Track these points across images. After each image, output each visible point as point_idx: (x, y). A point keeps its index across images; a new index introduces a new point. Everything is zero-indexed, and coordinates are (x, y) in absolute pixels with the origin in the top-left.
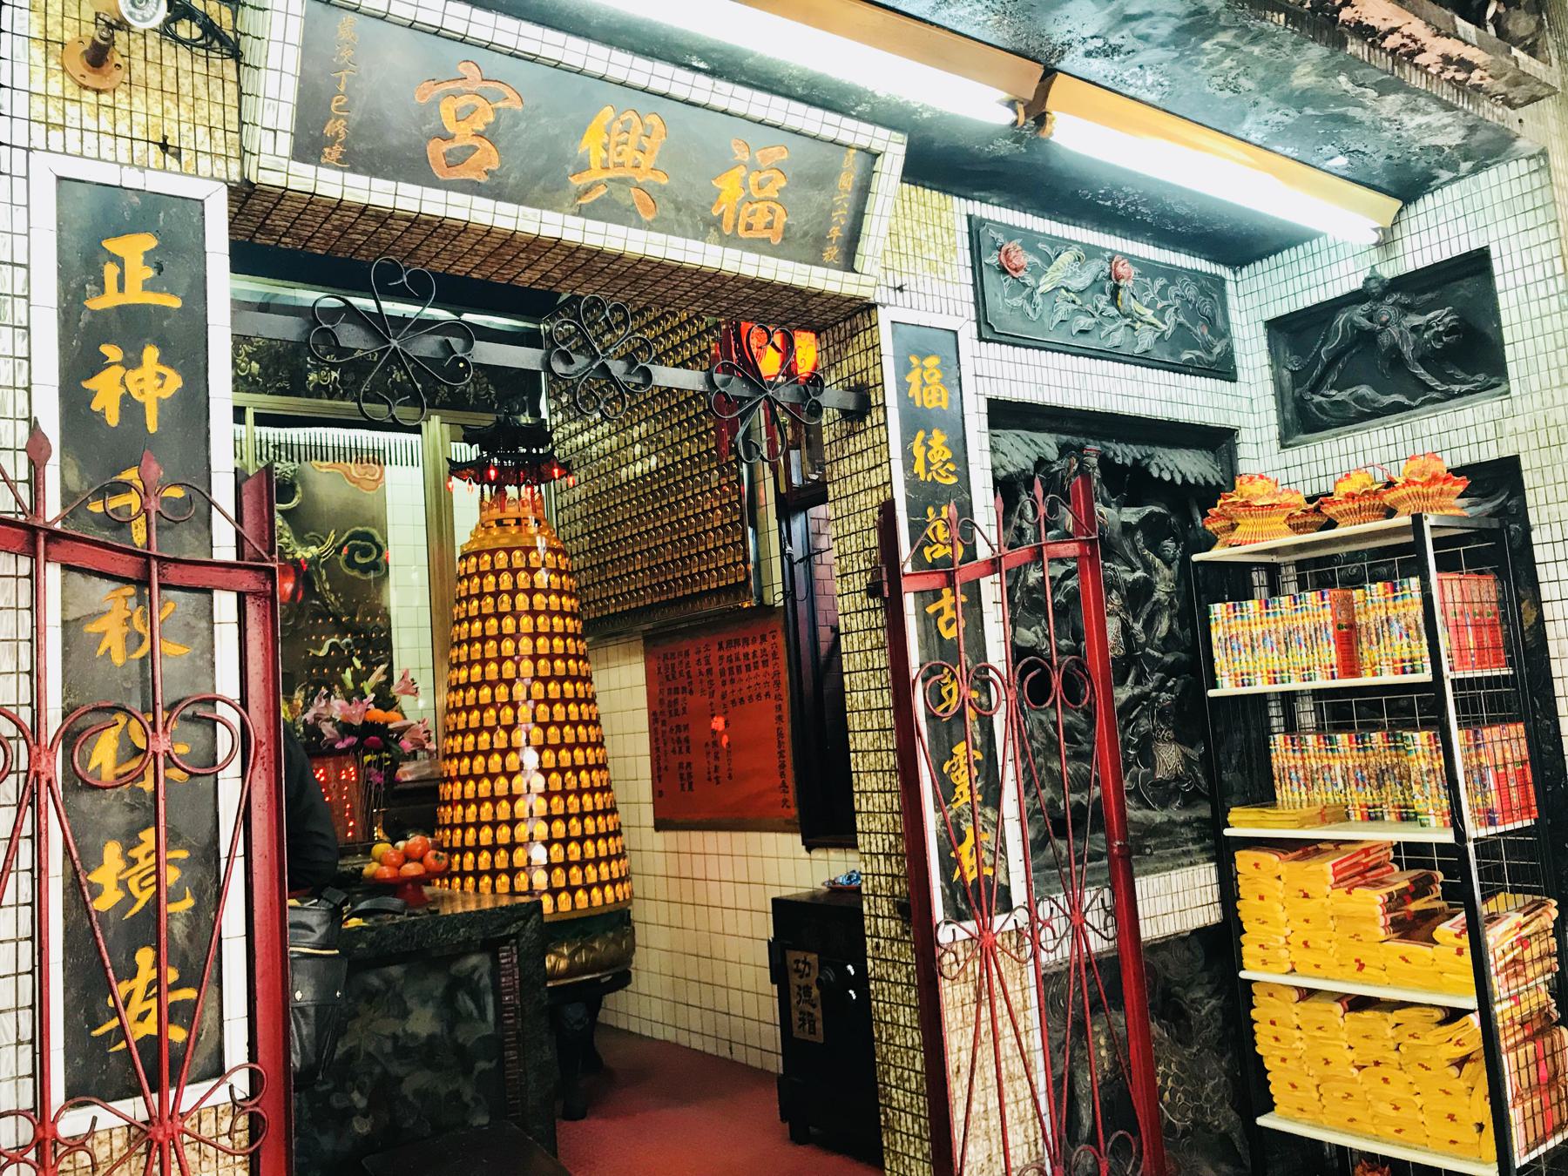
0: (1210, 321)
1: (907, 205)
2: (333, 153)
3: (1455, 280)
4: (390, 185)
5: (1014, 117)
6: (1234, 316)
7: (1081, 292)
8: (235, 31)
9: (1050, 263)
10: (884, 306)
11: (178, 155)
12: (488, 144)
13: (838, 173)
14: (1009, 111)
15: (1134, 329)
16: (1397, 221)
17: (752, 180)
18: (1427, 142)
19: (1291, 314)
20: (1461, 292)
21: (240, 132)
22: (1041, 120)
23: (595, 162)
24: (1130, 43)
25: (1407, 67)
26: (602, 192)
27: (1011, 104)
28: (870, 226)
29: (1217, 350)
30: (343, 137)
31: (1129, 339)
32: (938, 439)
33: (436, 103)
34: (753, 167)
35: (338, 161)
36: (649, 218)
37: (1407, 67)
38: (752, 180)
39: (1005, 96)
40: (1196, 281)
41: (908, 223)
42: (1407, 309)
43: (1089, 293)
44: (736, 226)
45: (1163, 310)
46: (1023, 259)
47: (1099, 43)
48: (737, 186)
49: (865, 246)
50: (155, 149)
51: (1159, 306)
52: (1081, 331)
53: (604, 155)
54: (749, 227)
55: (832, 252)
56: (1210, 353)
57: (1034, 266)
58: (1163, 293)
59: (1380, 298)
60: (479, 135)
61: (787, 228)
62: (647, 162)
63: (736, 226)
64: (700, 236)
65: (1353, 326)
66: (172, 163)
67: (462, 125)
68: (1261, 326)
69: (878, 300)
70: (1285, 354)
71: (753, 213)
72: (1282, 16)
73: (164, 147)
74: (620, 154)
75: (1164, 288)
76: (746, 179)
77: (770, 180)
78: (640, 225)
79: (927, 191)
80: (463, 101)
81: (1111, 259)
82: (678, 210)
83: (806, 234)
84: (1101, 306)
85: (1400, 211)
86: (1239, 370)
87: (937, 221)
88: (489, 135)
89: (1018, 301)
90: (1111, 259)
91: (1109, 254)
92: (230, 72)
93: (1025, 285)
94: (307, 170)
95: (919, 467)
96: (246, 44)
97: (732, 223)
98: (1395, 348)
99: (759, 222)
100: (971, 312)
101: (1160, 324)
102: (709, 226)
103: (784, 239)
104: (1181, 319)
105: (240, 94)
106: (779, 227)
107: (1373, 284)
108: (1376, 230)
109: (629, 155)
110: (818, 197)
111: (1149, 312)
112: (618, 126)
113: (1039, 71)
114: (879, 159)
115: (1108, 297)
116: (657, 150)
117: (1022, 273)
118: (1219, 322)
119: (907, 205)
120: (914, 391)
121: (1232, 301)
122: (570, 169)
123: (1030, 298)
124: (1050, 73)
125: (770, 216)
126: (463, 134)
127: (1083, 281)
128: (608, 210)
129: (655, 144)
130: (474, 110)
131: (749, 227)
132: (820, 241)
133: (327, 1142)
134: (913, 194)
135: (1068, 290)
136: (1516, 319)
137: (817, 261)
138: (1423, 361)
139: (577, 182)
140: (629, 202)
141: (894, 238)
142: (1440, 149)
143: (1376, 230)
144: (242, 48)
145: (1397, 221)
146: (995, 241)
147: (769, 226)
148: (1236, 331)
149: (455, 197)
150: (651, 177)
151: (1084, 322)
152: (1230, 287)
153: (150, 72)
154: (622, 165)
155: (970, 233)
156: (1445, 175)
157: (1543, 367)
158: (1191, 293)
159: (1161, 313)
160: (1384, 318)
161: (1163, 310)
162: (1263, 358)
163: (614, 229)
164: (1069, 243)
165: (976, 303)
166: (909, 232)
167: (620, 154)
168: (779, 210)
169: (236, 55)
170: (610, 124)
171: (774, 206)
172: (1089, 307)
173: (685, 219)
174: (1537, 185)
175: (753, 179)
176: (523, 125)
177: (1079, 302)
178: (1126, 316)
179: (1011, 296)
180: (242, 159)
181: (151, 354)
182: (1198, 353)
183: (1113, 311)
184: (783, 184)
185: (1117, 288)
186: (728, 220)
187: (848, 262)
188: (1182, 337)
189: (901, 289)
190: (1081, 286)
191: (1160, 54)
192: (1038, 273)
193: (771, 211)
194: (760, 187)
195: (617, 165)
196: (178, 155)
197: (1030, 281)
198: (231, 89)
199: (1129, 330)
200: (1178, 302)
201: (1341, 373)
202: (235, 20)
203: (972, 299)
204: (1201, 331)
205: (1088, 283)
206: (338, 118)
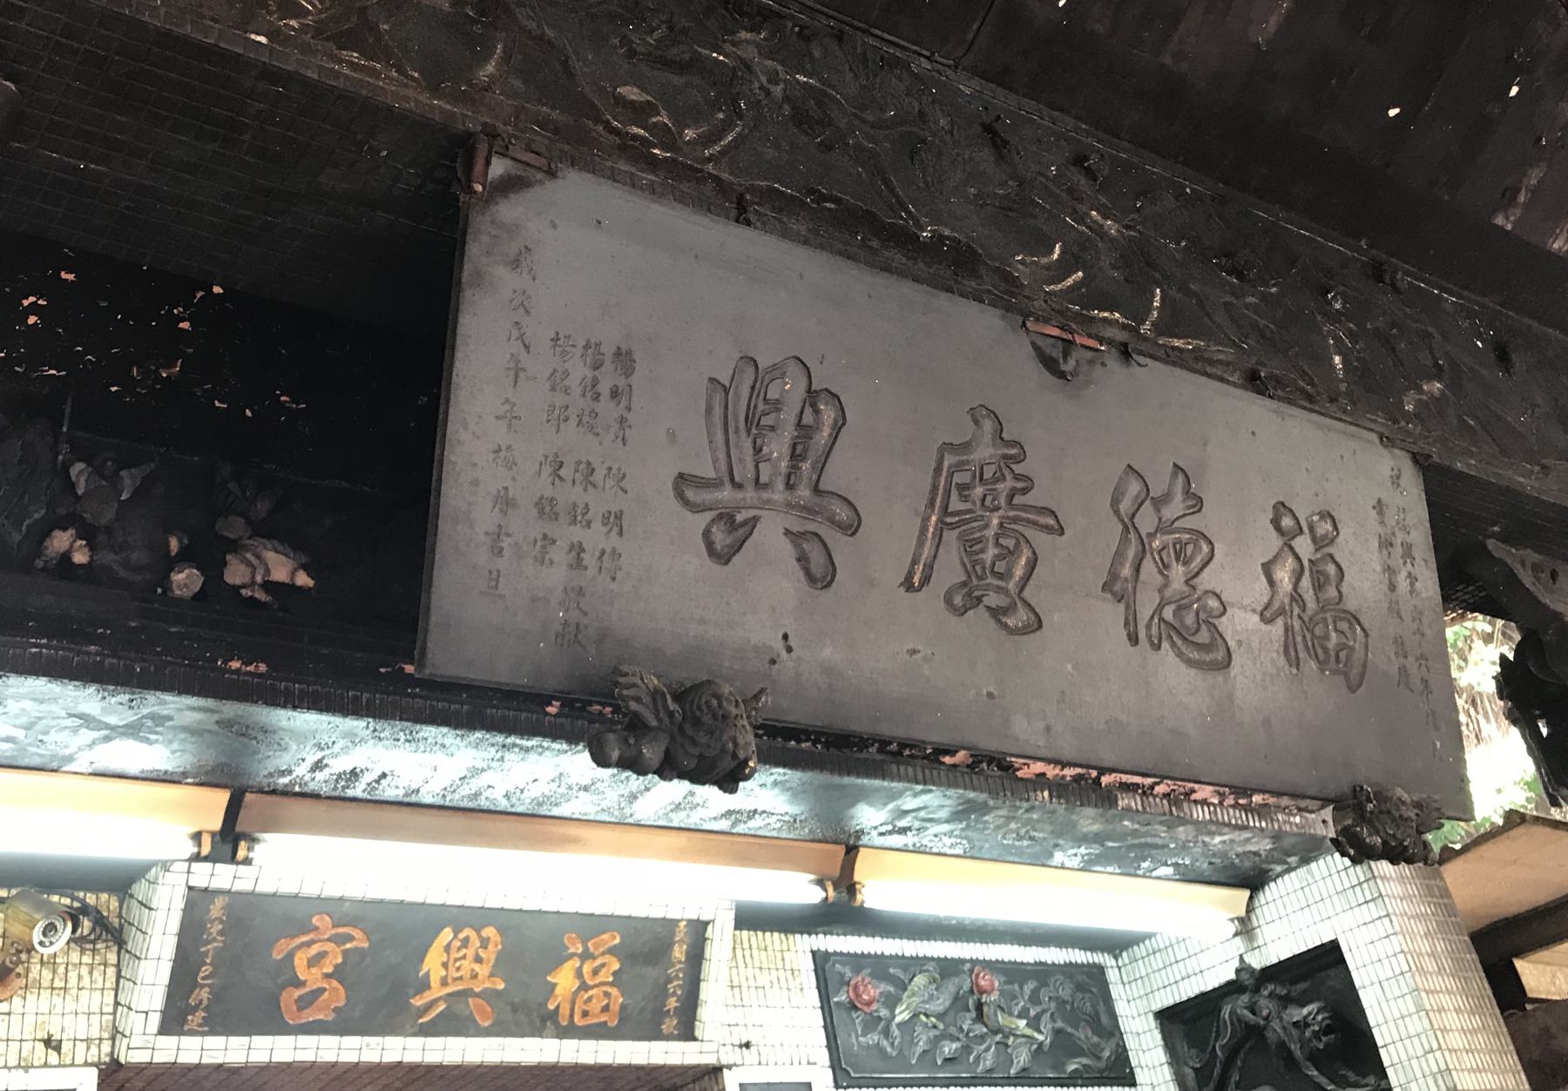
0: (1095, 1023)
1: (747, 952)
2: (194, 1020)
3: (1320, 970)
4: (242, 1041)
5: (824, 895)
6: (1121, 1008)
7: (940, 1016)
8: (120, 916)
9: (905, 989)
10: (729, 1067)
11: (58, 1049)
12: (335, 983)
13: (670, 946)
14: (818, 889)
15: (1007, 1046)
16: (1250, 909)
17: (587, 968)
18: (1240, 850)
19: (1176, 1005)
20: (1330, 983)
21: (114, 1013)
22: (852, 889)
23: (435, 980)
24: (917, 824)
25: (1185, 805)
26: (442, 1007)
27: (820, 883)
28: (706, 991)
29: (1106, 1054)
30: (205, 1002)
31: (1002, 1058)
33: (290, 956)
34: (586, 956)
35: (200, 1025)
36: (486, 1024)
37: (1185, 805)
38: (587, 968)
39: (813, 877)
40: (1071, 977)
41: (750, 972)
42: (1285, 1001)
43: (952, 1013)
44: (572, 1010)
45: (1038, 1017)
46: (873, 991)
47: (890, 827)
49: (703, 1013)
50: (40, 1046)
51: (1032, 1013)
52: (946, 1060)
53: (443, 973)
54: (585, 1014)
55: (669, 1025)
56: (1099, 1058)
57: (887, 995)
58: (1035, 999)
59: (1256, 990)
60: (327, 976)
61: (623, 1007)
62: (483, 970)
63: (572, 1016)
64: (537, 1032)
65: (1239, 1021)
66: (53, 1057)
67: (314, 970)
68: (1151, 1016)
69: (724, 1062)
70: (1182, 1047)
71: (590, 999)
72: (1046, 794)
73: (48, 1042)
74: (458, 969)
75: (1035, 992)
76: (580, 968)
77: (603, 965)
79: (768, 934)
80: (314, 950)
81: (971, 971)
82: (515, 1010)
83: (643, 1010)
84: (965, 1027)
85: (1251, 898)
86: (1138, 1072)
87: (780, 965)
88: (338, 974)
89: (873, 1038)
90: (971, 971)
91: (968, 966)
92: (112, 957)
93: (880, 1019)
94: (170, 1041)
96: (132, 935)
97: (568, 1013)
98: (1282, 1045)
99: (595, 1006)
100: (823, 1057)
101: (1036, 1035)
102: (544, 1022)
103: (621, 1020)
104: (1059, 1024)
105: (119, 976)
106: (615, 1008)
107: (1245, 976)
108: (1232, 920)
109: (467, 965)
110: (652, 973)
111: (1022, 1023)
113: (841, 850)
114: (710, 928)
115: (974, 1014)
116: (493, 957)
117: (874, 1007)
118: (1104, 1019)
119: (747, 952)
121: (1116, 991)
122: (411, 992)
123: (886, 1033)
124: (852, 851)
125: (606, 998)
126: (312, 978)
127: (941, 1003)
128: (453, 1023)
129: (490, 955)
131: (585, 1014)
132: (660, 1014)
133: (991, 803)
134: (753, 939)
135: (927, 1016)
136: (1381, 1021)
137: (657, 1035)
138: (1314, 1058)
139: (418, 1002)
140: (467, 1013)
141: (737, 990)
142: (1256, 854)
143: (1232, 920)
144: (125, 936)
145: (1250, 909)
146: (842, 975)
147: (606, 1009)
148: (1126, 1025)
149: (304, 1040)
150: (487, 985)
151: (949, 1048)
152: (1112, 975)
153: (44, 972)
154: (461, 978)
155: (816, 971)
156: (1279, 868)
157: (1419, 1075)
158: (1065, 992)
159: (1034, 1024)
160: (1265, 1013)
161: (1038, 1017)
162: (1159, 1055)
163: (453, 1042)
164: (918, 963)
165: (829, 1047)
166: (752, 982)
167: (458, 969)
168: (614, 991)
169: (121, 943)
170: (449, 945)
171: (609, 989)
172: (952, 1030)
173: (523, 1018)
174: (1362, 879)
175: (587, 968)
176: (368, 960)
177: (941, 1026)
178: (995, 1033)
179: (864, 1035)
180: (113, 1039)
182: (1085, 1061)
183: (980, 1029)
184: (616, 966)
185: (979, 1007)
186: (565, 1010)
187: (687, 1032)
188: (1064, 1045)
189: (747, 1045)
190: (941, 1009)
191: (946, 827)
192: (892, 1002)
193: (607, 994)
194: (595, 972)
195: (455, 979)
196: (58, 1049)
197: (884, 1013)
198: (111, 971)
199: (1001, 1047)
200: (1053, 1005)
201: (1241, 1070)
202: (121, 907)
203: (824, 1043)
204: (1084, 1035)
205: (948, 1003)
206: (203, 986)
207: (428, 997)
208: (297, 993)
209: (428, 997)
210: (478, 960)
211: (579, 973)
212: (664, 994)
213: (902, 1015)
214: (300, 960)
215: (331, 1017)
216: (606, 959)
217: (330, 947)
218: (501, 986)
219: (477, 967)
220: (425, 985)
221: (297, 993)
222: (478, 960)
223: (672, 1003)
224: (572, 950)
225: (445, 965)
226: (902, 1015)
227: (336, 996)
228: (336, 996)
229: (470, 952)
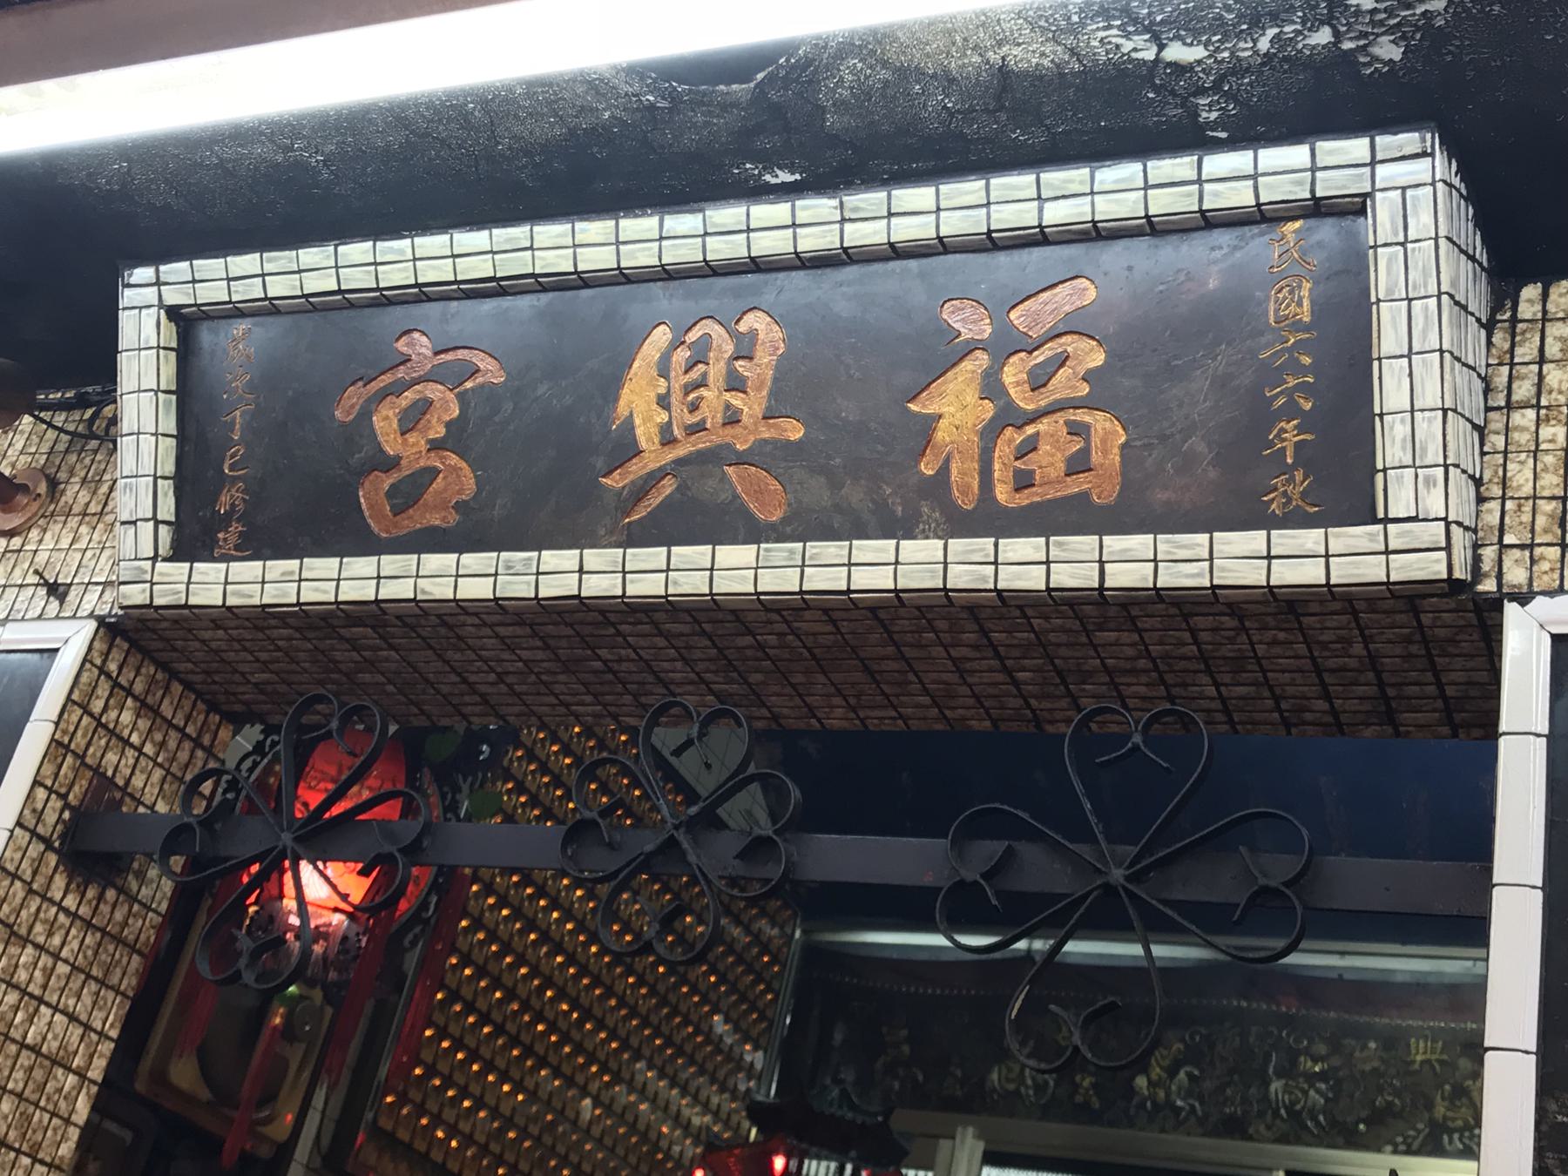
10: (1523, 598)
11: (62, 599)
12: (453, 459)
26: (668, 486)
33: (365, 415)
48: (971, 397)
60: (435, 446)
62: (750, 406)
64: (900, 527)
69: (1516, 575)
78: (754, 533)
82: (835, 484)
88: (456, 438)
99: (1050, 460)
112: (682, 355)
126: (411, 450)
130: (425, 406)
147: (1079, 465)
175: (1013, 374)
176: (508, 407)
207: (638, 468)
208: (387, 481)
209: (638, 468)
210: (735, 384)
211: (991, 387)
212: (1261, 418)
214: (385, 422)
215: (453, 518)
216: (1070, 344)
217: (434, 391)
218: (795, 431)
219: (736, 400)
220: (627, 449)
221: (387, 481)
222: (735, 384)
223: (1289, 435)
224: (966, 335)
225: (663, 402)
229: (716, 371)
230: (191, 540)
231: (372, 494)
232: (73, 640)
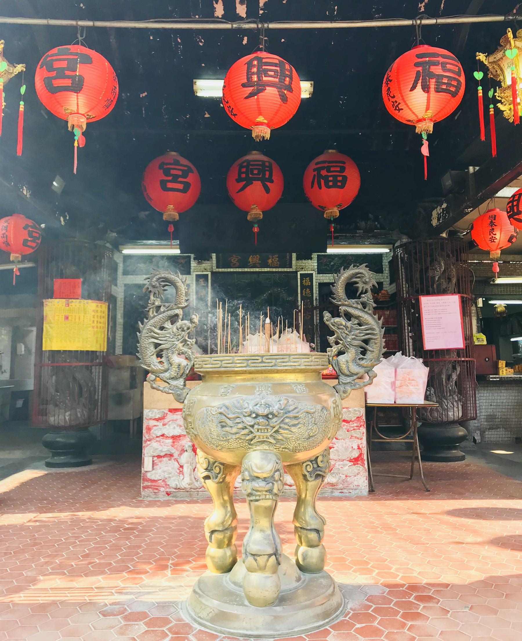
32: (308, 290)
95: (304, 294)
120: (304, 283)
126: (235, 262)
129: (258, 258)
181: (481, 57)
192: (330, 262)
213: (332, 263)
214: (232, 260)
220: (250, 262)
226: (332, 263)
227: (238, 264)
228: (238, 264)
230: (218, 267)
231: (232, 264)
232: (209, 274)
